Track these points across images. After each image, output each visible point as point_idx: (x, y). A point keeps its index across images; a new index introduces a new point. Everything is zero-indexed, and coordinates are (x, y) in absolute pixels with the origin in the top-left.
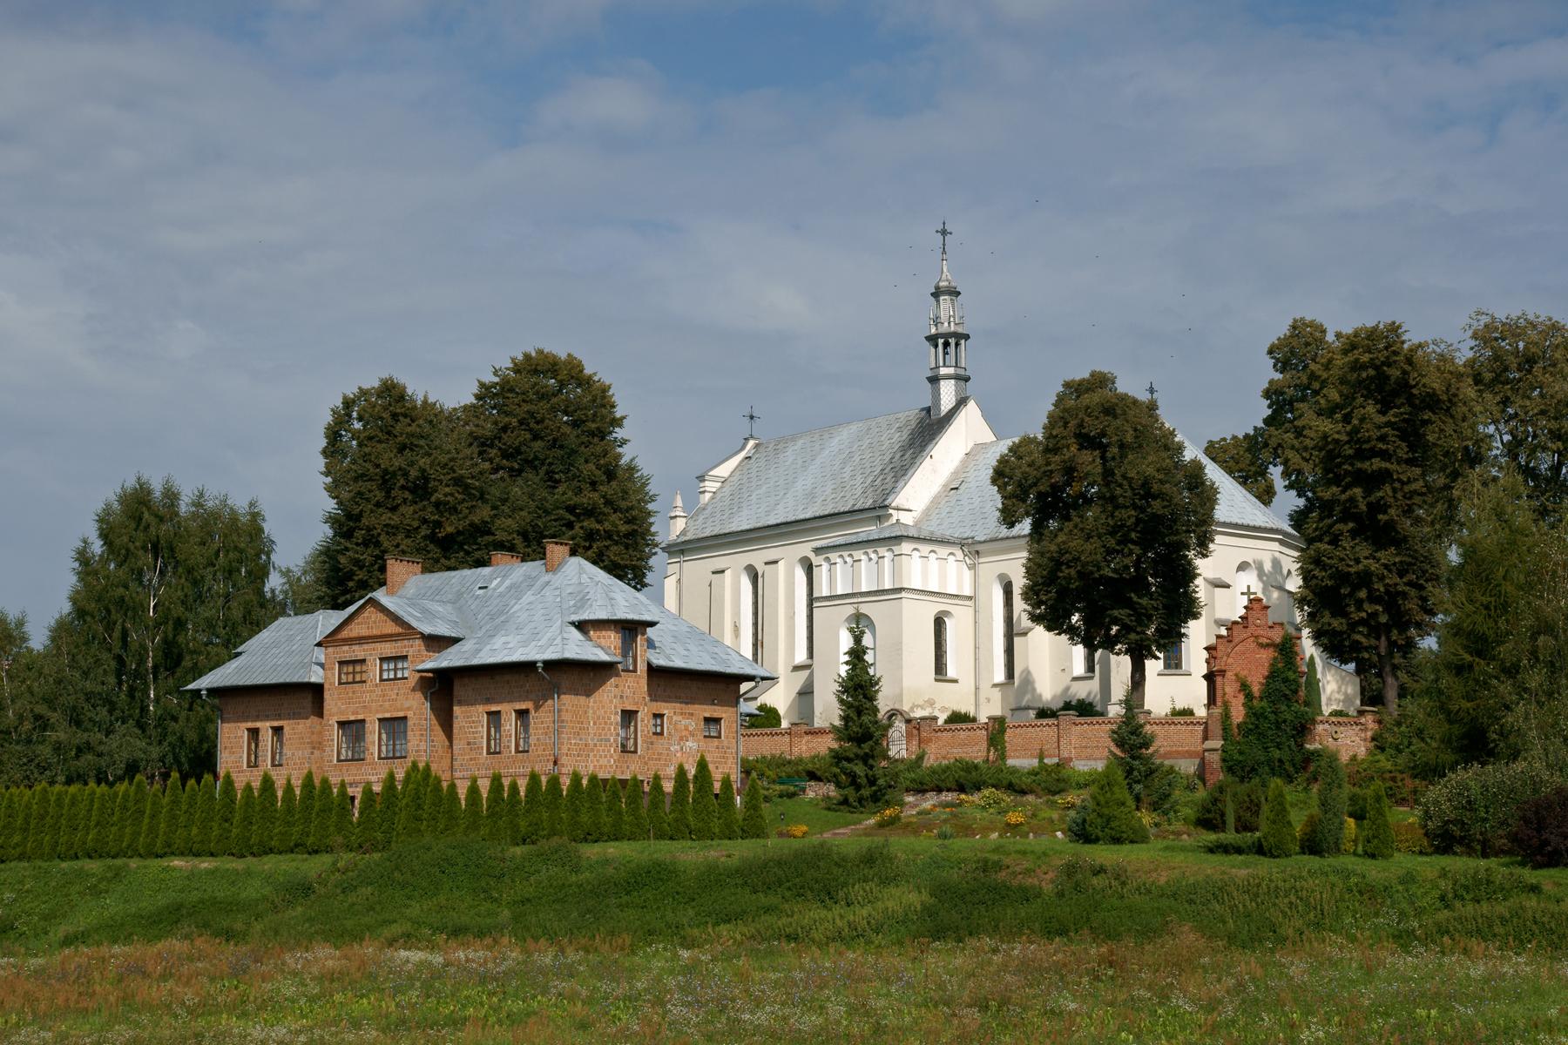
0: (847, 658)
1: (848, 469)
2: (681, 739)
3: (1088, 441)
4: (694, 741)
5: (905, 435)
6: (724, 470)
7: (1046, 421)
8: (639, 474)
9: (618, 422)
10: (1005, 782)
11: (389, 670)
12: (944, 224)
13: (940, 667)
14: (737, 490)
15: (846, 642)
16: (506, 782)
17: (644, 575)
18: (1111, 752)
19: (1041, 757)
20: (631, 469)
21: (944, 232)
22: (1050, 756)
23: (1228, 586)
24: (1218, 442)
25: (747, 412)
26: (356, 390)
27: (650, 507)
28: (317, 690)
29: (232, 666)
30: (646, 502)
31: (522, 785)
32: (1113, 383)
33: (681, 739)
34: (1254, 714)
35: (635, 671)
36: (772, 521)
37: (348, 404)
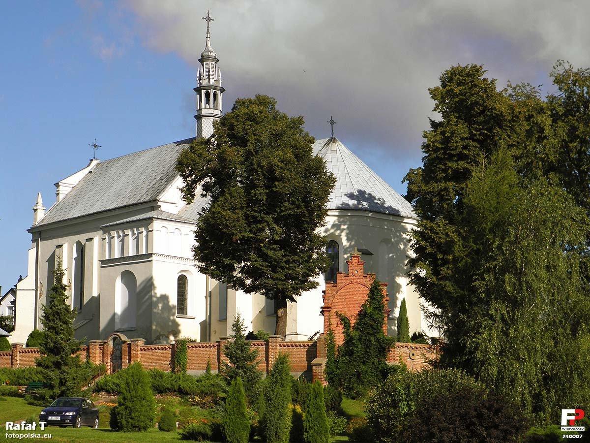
1: (143, 177)
3: (240, 141)
6: (75, 179)
10: (176, 388)
12: (208, 13)
14: (79, 193)
19: (208, 369)
21: (208, 19)
23: (372, 254)
25: (92, 142)
34: (349, 341)
36: (92, 212)
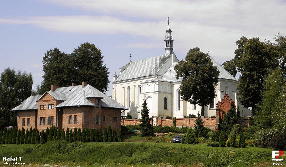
0: (143, 105)
2: (109, 121)
4: (111, 122)
5: (160, 60)
7: (44, 73)
8: (106, 68)
9: (102, 58)
11: (42, 108)
13: (165, 108)
15: (143, 102)
16: (70, 130)
17: (107, 88)
18: (195, 125)
20: (104, 67)
22: (185, 126)
24: (226, 62)
26: (50, 50)
27: (108, 75)
28: (36, 111)
29: (20, 106)
30: (107, 74)
31: (73, 130)
32: (200, 50)
33: (109, 121)
35: (99, 108)
37: (48, 53)
